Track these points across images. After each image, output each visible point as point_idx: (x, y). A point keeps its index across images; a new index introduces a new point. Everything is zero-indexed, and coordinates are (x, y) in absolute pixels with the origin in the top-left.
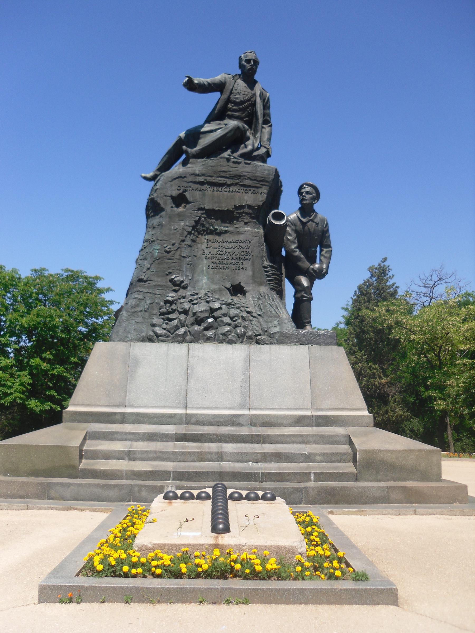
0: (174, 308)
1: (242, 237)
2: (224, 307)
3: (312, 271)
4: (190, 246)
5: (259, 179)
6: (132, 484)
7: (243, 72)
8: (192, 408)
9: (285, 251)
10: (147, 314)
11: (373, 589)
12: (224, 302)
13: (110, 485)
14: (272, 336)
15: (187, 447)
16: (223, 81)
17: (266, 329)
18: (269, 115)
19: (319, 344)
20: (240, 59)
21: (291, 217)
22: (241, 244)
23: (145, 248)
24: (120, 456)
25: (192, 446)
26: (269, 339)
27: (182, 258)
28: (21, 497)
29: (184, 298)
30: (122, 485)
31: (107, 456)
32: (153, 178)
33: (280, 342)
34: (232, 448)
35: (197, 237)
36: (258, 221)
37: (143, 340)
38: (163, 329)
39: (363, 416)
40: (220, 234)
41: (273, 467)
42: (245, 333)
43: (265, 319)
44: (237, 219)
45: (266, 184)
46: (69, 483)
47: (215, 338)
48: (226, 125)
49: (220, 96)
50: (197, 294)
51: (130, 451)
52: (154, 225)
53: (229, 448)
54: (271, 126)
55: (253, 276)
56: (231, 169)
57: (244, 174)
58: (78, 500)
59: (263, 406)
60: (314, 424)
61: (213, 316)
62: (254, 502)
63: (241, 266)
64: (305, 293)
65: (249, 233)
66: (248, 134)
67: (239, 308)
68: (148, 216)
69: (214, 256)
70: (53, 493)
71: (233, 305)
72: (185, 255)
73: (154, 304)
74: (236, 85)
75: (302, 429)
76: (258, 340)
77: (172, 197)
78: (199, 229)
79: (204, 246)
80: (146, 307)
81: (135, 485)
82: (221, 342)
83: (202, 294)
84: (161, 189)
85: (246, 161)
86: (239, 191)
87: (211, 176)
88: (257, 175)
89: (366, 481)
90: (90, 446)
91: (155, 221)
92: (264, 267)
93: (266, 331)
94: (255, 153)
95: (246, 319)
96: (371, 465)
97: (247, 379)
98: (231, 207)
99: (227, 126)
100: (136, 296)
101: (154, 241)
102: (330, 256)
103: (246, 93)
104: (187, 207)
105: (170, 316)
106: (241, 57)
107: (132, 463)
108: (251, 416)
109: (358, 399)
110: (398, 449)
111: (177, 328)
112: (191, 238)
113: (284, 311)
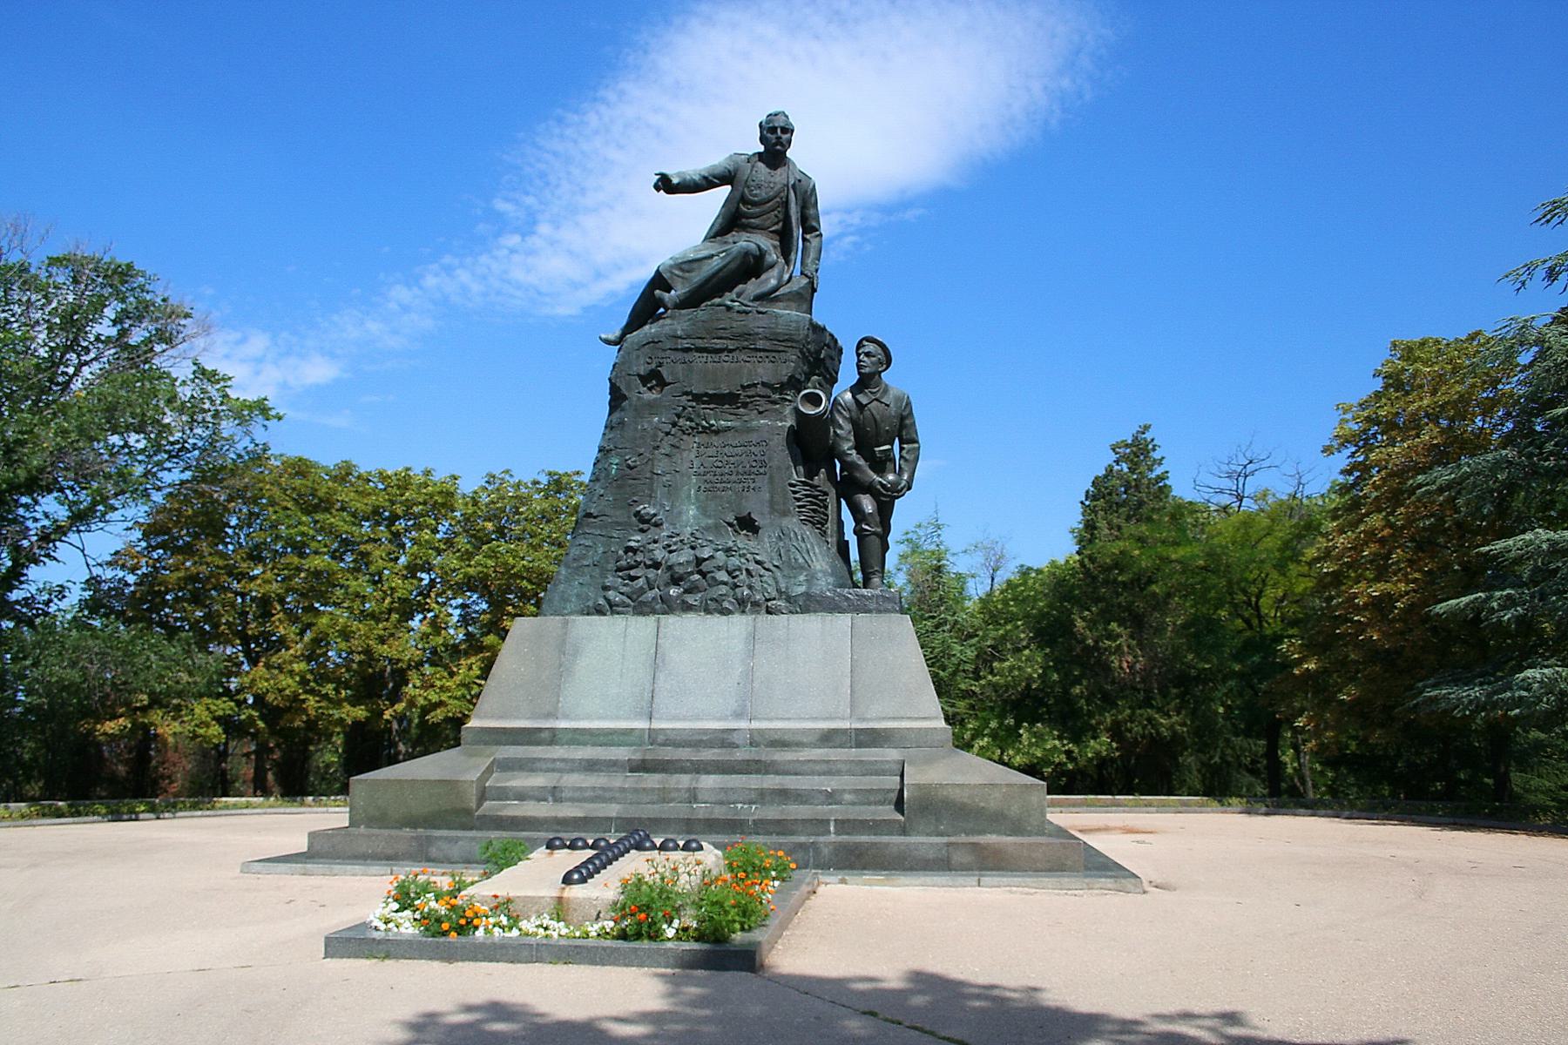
1: (754, 438)
10: (597, 570)
22: (753, 449)
24: (539, 796)
28: (388, 858)
31: (521, 796)
32: (618, 342)
33: (805, 610)
41: (772, 812)
83: (686, 536)
89: (919, 834)
97: (749, 674)
102: (917, 459)
105: (632, 573)
107: (559, 806)
111: (642, 591)
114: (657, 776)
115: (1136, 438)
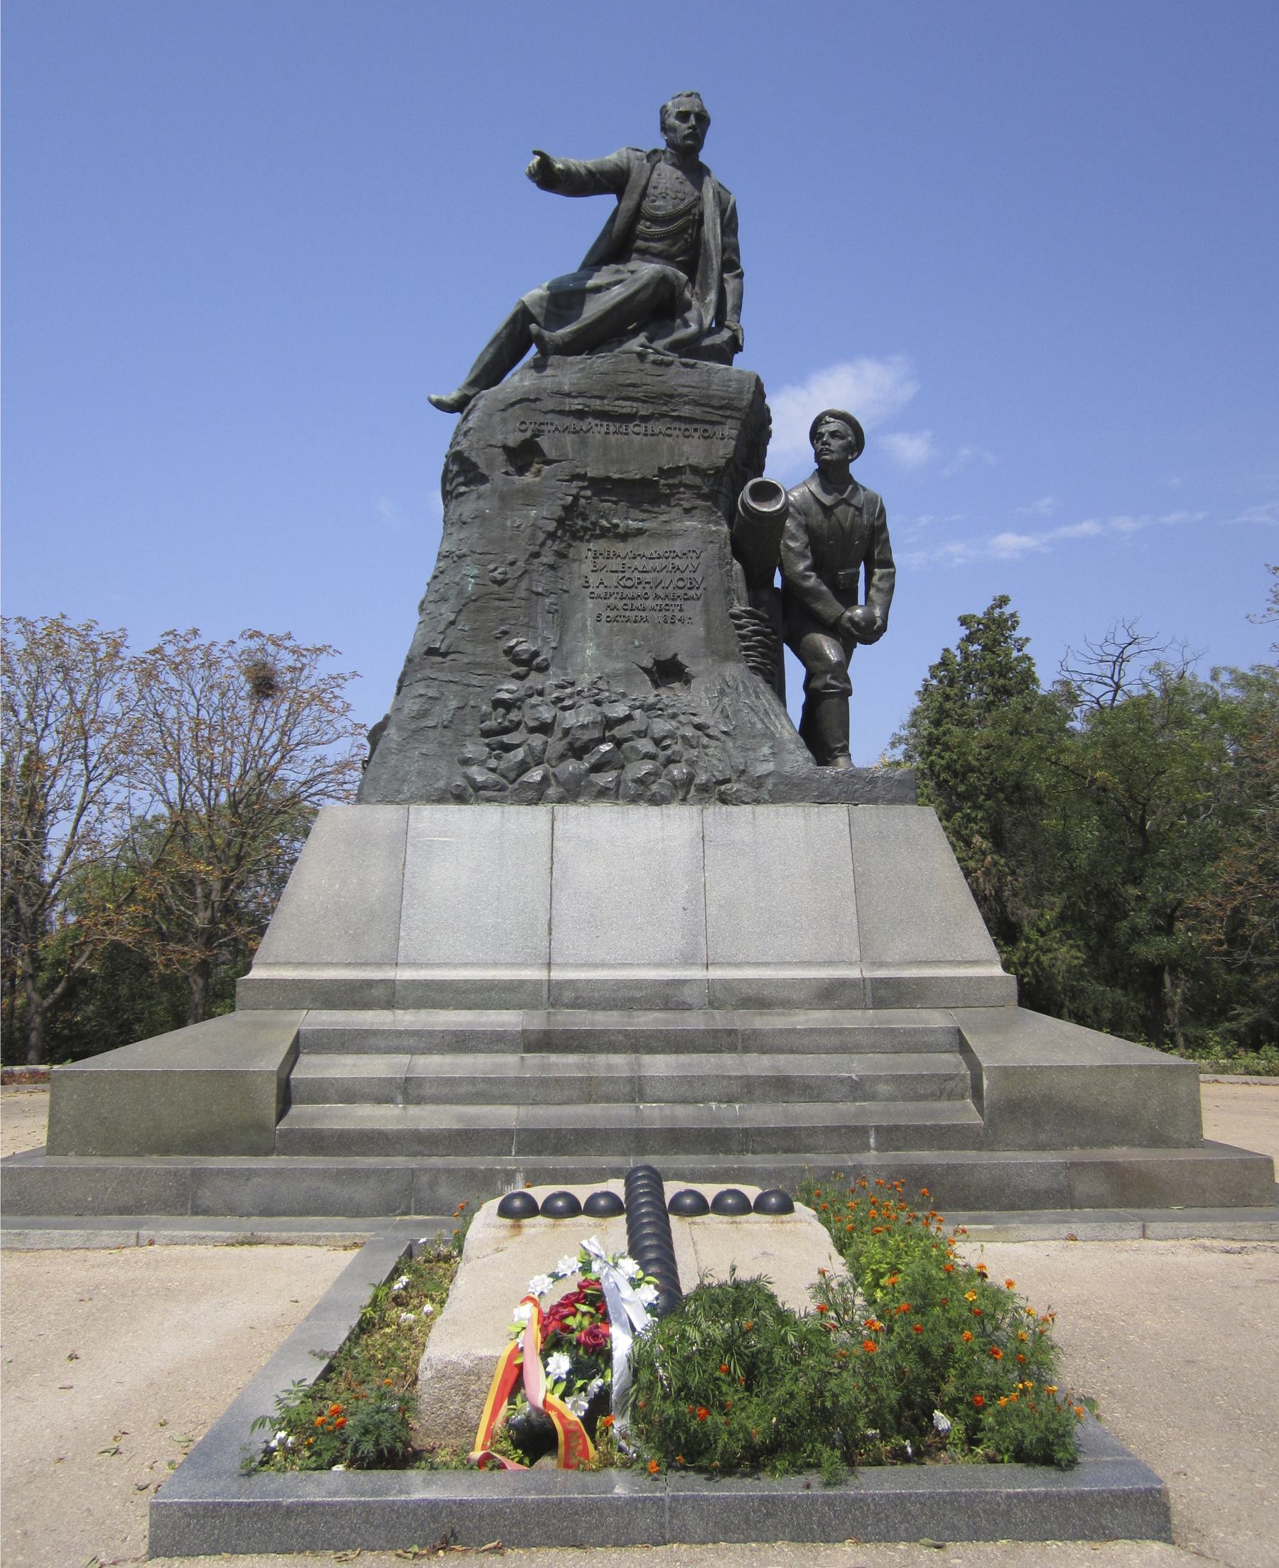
0: (516, 719)
1: (678, 545)
2: (637, 713)
3: (848, 625)
4: (552, 567)
5: (715, 403)
6: (414, 1166)
7: (670, 144)
8: (565, 965)
9: (782, 574)
10: (449, 733)
11: (1099, 1493)
12: (638, 704)
13: (357, 1171)
14: (758, 782)
15: (550, 1066)
16: (624, 166)
17: (742, 768)
18: (736, 250)
19: (874, 801)
20: (664, 111)
21: (796, 494)
22: (677, 562)
23: (442, 572)
24: (381, 1092)
25: (566, 1063)
26: (750, 790)
27: (534, 597)
28: (123, 1210)
29: (541, 693)
30: (389, 1171)
32: (459, 406)
33: (777, 798)
34: (667, 1065)
35: (570, 546)
36: (716, 504)
37: (441, 798)
38: (493, 770)
39: (992, 978)
40: (625, 536)
42: (691, 778)
43: (739, 743)
44: (665, 499)
45: (734, 414)
46: (248, 1169)
47: (617, 790)
48: (632, 272)
49: (616, 203)
50: (572, 684)
51: (407, 1080)
52: (464, 519)
53: (659, 1065)
54: (741, 276)
55: (708, 639)
56: (649, 380)
57: (681, 390)
58: (273, 1215)
59: (741, 957)
60: (869, 1000)
61: (613, 736)
62: (738, 1218)
63: (678, 615)
64: (832, 678)
65: (695, 534)
66: (687, 294)
67: (674, 716)
68: (447, 495)
69: (611, 591)
70: (206, 1196)
71: (660, 709)
72: (540, 590)
73: (468, 709)
74: (655, 175)
75: (838, 1013)
76: (724, 793)
77: (505, 448)
78: (572, 526)
79: (587, 567)
80: (447, 716)
81: (420, 1170)
82: (634, 800)
83: (584, 681)
84: (479, 429)
85: (683, 360)
86: (669, 432)
87: (602, 398)
88: (711, 392)
89: (1008, 1147)
90: (310, 1068)
91: (467, 508)
92: (734, 616)
93: (743, 772)
94: (707, 342)
95: (694, 743)
96: (1028, 1109)
98: (650, 473)
99: (636, 276)
100: (422, 691)
101: (464, 556)
102: (892, 588)
103: (680, 195)
104: (543, 473)
105: (506, 739)
106: (664, 107)
107: (413, 1110)
108: (710, 983)
109: (978, 938)
110: (1088, 1063)
111: (523, 767)
112: (555, 548)
113: (785, 722)
114: (572, 1059)
115: (989, 613)
